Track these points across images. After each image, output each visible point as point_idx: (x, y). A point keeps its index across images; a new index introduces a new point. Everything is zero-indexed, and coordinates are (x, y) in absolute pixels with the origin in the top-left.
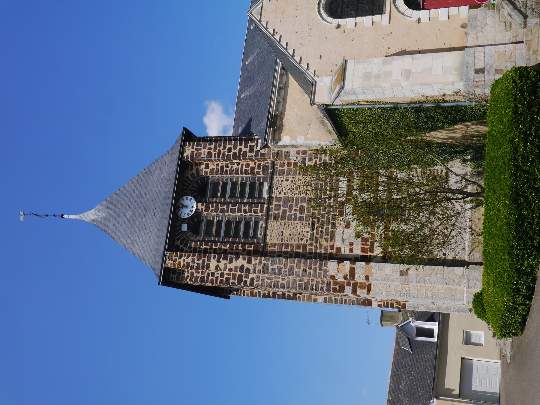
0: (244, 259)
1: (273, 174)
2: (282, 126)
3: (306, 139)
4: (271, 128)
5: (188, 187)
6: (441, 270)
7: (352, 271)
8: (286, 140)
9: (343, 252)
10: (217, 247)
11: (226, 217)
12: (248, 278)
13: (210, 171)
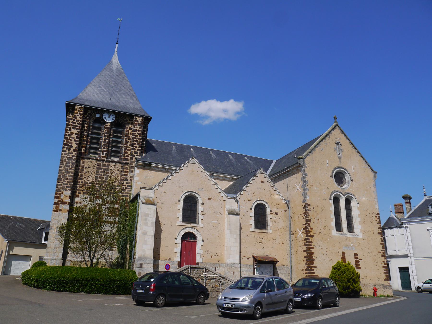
0: (76, 148)
1: (122, 163)
2: (145, 169)
3: (137, 182)
4: (144, 164)
5: (120, 118)
6: (62, 247)
7: (65, 203)
8: (137, 171)
9: (76, 198)
10: (85, 133)
11: (102, 138)
12: (66, 149)
13: (128, 130)
